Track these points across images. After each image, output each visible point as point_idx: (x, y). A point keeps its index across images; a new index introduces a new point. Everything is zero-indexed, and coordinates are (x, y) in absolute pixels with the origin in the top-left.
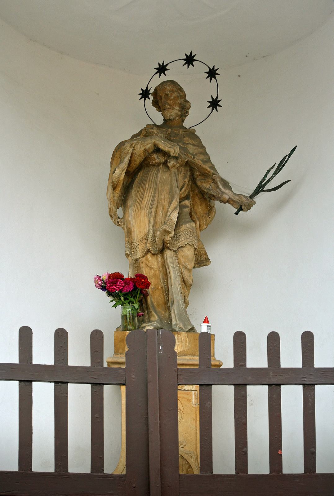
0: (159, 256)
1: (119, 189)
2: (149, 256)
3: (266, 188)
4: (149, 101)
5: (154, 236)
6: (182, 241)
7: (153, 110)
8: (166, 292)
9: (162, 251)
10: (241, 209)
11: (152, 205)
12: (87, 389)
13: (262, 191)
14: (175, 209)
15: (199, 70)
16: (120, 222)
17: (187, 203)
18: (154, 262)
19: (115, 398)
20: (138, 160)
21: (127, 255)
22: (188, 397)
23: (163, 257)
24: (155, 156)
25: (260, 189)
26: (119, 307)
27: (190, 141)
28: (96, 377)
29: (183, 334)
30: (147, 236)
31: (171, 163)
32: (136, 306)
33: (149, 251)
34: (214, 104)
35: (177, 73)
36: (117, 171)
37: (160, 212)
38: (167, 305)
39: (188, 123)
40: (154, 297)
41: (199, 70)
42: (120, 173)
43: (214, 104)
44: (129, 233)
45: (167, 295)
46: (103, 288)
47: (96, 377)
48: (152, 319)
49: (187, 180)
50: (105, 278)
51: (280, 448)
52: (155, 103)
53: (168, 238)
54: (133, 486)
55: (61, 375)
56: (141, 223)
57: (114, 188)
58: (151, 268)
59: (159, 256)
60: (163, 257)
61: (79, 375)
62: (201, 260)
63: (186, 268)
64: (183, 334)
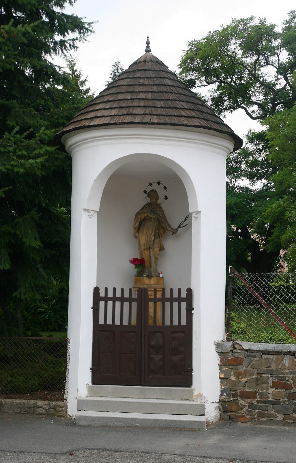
0: (148, 250)
1: (137, 229)
2: (145, 250)
3: (181, 226)
4: (146, 195)
5: (147, 244)
6: (155, 246)
7: (148, 198)
8: (150, 262)
9: (149, 249)
10: (173, 233)
11: (146, 233)
12: (128, 303)
13: (180, 227)
14: (153, 236)
15: (161, 186)
16: (136, 237)
17: (157, 231)
18: (147, 252)
19: (134, 305)
20: (142, 219)
21: (139, 250)
22: (151, 304)
23: (149, 251)
24: (147, 217)
25: (179, 227)
26: (136, 269)
27: (159, 210)
28: (130, 300)
29: (155, 278)
30: (145, 244)
31: (152, 220)
32: (141, 268)
33: (145, 249)
34: (166, 198)
35: (155, 187)
36: (136, 224)
37: (149, 236)
38: (150, 267)
39: (158, 202)
40: (147, 264)
41: (161, 186)
42: (137, 225)
43: (166, 198)
44: (139, 242)
45: (151, 263)
46: (132, 263)
47: (130, 300)
48: (146, 271)
49: (157, 224)
50: (132, 260)
51: (172, 319)
52: (148, 196)
53: (151, 246)
54: (153, 343)
55: (122, 300)
56: (143, 240)
57: (135, 229)
58: (146, 254)
59: (148, 250)
60: (149, 251)
61: (126, 300)
62: (162, 249)
63: (156, 254)
64: (155, 278)
